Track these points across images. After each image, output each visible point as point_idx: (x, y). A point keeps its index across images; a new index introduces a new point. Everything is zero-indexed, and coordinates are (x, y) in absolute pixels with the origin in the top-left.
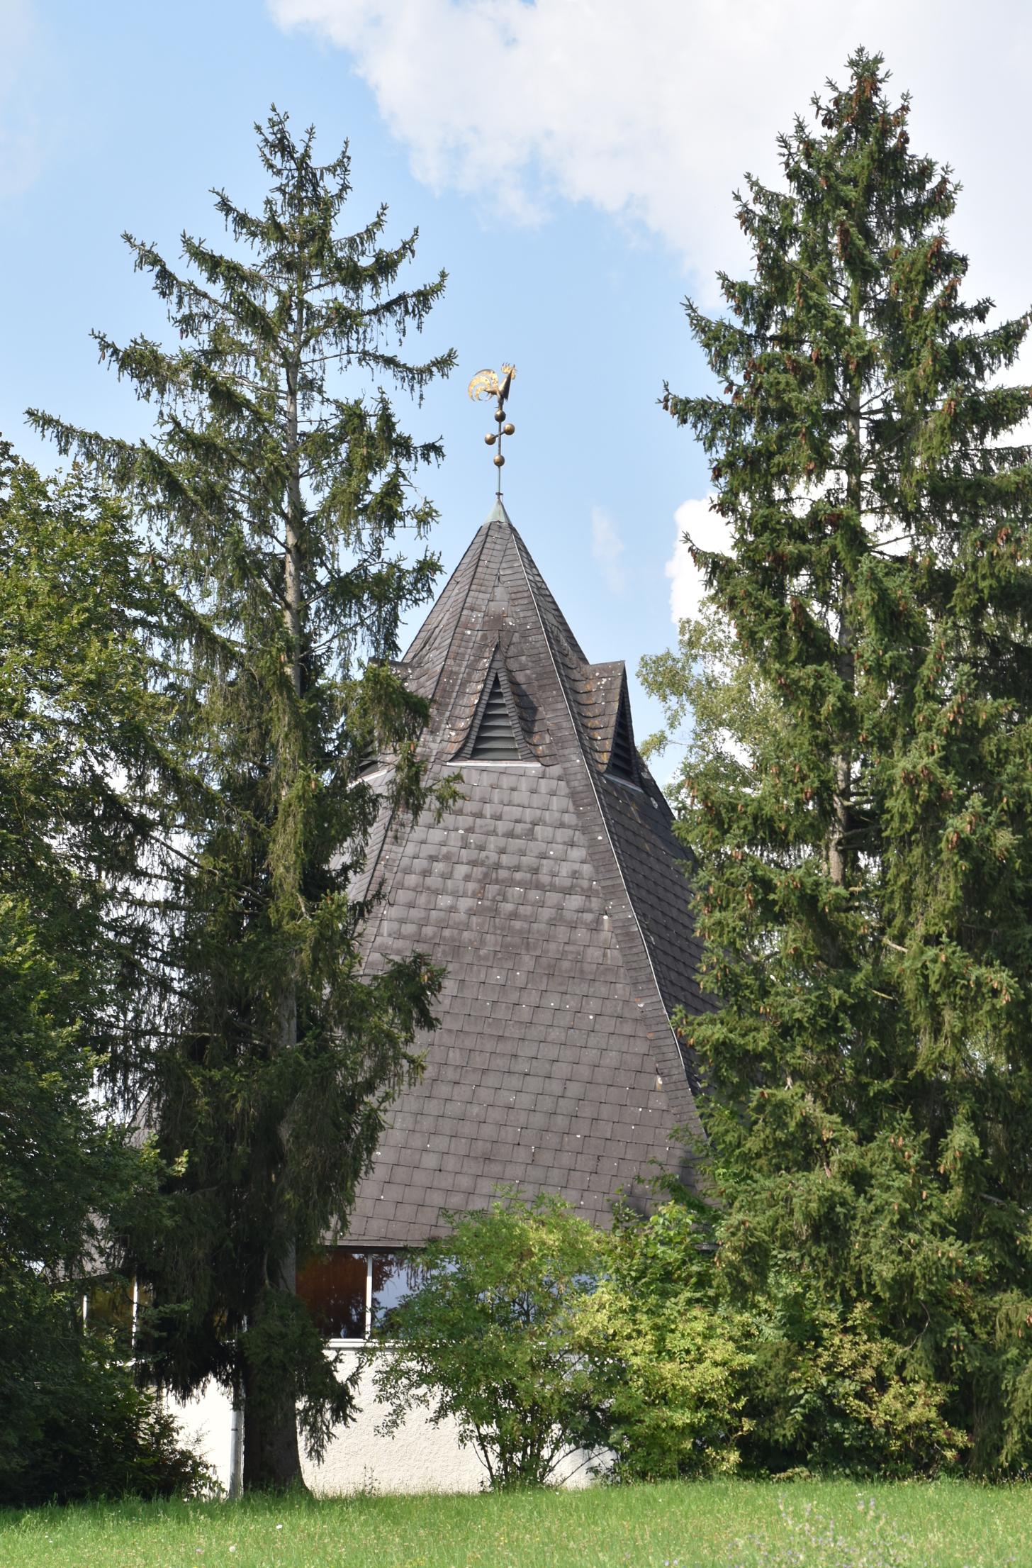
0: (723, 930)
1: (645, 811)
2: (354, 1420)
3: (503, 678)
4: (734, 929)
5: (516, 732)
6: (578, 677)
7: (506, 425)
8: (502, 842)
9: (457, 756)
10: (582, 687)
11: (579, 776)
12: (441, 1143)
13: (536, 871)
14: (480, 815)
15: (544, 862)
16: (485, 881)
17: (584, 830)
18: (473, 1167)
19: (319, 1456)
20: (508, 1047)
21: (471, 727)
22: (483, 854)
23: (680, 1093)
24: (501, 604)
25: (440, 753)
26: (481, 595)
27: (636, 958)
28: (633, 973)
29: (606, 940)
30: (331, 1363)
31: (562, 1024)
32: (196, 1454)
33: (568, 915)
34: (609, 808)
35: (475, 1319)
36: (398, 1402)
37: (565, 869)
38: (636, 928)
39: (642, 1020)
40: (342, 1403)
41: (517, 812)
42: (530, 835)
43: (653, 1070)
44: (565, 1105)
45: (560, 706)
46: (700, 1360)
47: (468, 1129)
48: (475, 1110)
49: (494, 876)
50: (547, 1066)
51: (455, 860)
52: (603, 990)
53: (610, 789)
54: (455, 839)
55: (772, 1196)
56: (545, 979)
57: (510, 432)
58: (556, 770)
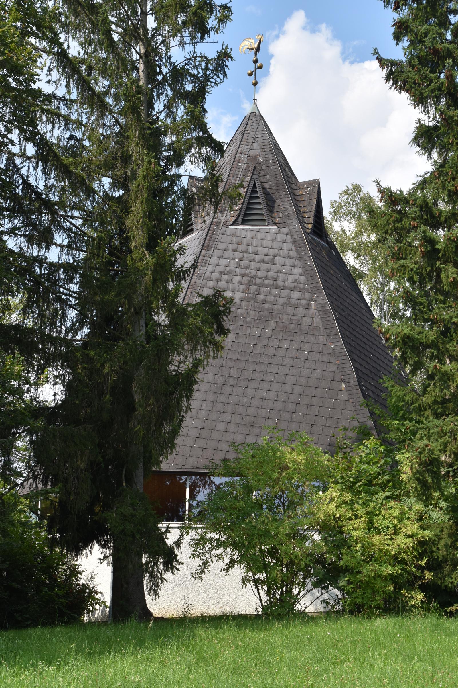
0: (405, 270)
1: (329, 255)
2: (178, 570)
3: (258, 184)
4: (412, 270)
5: (265, 211)
6: (295, 188)
7: (259, 64)
8: (258, 265)
9: (234, 223)
10: (297, 192)
11: (297, 233)
12: (227, 417)
13: (276, 279)
14: (246, 252)
15: (280, 275)
16: (249, 284)
17: (300, 259)
18: (245, 430)
19: (156, 593)
20: (263, 368)
21: (242, 208)
22: (248, 271)
23: (355, 392)
24: (256, 150)
25: (226, 221)
26: (246, 147)
27: (329, 323)
28: (327, 330)
29: (313, 314)
30: (163, 533)
31: (291, 356)
32: (91, 586)
33: (293, 301)
34: (313, 250)
35: (252, 507)
36: (205, 558)
37: (291, 278)
38: (329, 308)
39: (333, 354)
40: (170, 559)
41: (265, 250)
42: (272, 262)
43: (340, 380)
44: (293, 398)
45: (287, 199)
46: (396, 533)
47: (241, 410)
48: (245, 400)
49: (254, 282)
50: (283, 378)
51: (233, 274)
52: (312, 339)
53: (313, 241)
54: (233, 264)
55: (442, 431)
56: (281, 334)
57: (260, 67)
58: (285, 230)
